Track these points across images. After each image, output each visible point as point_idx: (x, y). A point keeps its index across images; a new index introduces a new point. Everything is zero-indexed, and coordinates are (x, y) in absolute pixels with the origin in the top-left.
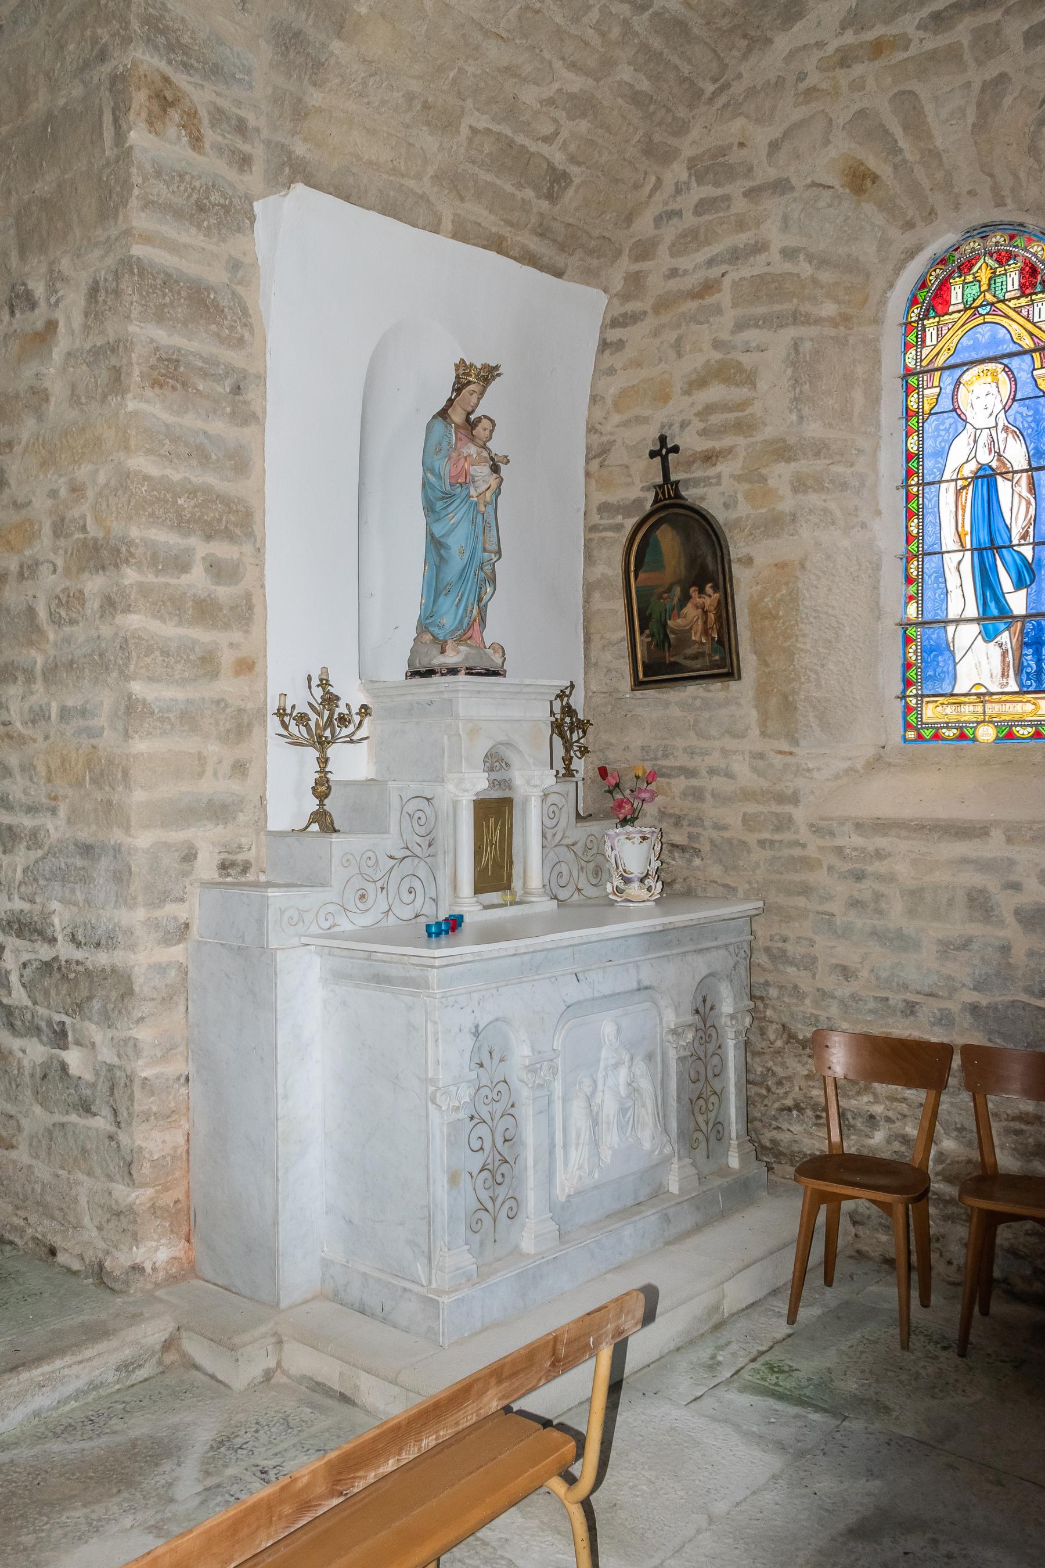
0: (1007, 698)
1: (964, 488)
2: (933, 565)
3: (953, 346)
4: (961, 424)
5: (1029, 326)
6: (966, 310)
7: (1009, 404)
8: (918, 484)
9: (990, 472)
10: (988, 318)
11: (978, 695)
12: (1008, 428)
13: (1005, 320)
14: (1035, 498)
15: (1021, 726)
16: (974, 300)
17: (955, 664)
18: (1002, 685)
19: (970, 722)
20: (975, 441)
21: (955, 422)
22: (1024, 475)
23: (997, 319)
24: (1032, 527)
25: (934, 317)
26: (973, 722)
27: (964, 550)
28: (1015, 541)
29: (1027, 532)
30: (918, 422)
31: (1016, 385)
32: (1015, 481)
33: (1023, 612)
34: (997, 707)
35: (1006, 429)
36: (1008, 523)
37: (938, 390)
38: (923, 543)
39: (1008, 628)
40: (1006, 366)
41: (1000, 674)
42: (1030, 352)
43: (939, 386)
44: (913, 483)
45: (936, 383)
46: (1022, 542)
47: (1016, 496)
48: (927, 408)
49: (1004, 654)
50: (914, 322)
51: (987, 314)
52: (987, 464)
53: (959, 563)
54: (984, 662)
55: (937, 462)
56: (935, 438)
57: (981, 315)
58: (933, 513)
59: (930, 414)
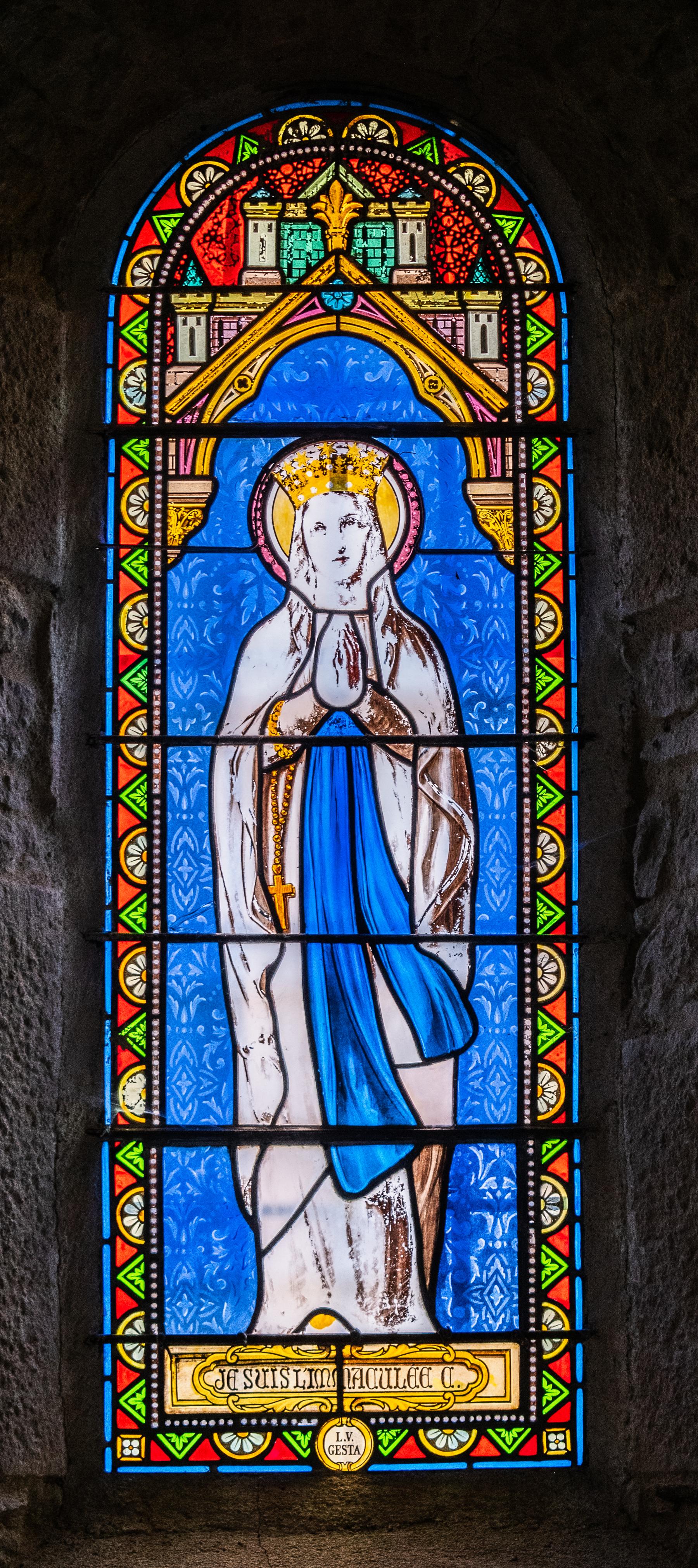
0: (402, 1350)
1: (280, 765)
2: (194, 971)
3: (256, 374)
4: (270, 591)
5: (458, 366)
6: (285, 289)
7: (402, 558)
8: (148, 740)
9: (352, 731)
10: (350, 324)
11: (323, 1341)
12: (400, 619)
13: (394, 337)
14: (475, 819)
15: (441, 1426)
16: (310, 270)
17: (260, 1254)
18: (388, 1317)
19: (300, 1416)
20: (314, 643)
21: (258, 581)
22: (446, 751)
23: (373, 331)
24: (467, 896)
25: (199, 291)
26: (309, 1416)
27: (280, 937)
28: (424, 929)
29: (455, 906)
30: (149, 564)
31: (421, 508)
32: (423, 762)
33: (446, 1121)
34: (375, 1375)
35: (394, 622)
36: (404, 874)
37: (205, 487)
38: (163, 907)
39: (406, 1163)
40: (394, 455)
41: (382, 1287)
42: (461, 431)
43: (211, 477)
44: (133, 732)
45: (202, 468)
46: (443, 931)
47: (425, 808)
48: (176, 531)
49: (394, 1234)
50: (143, 291)
51: (347, 311)
52: (347, 710)
53: (270, 971)
54: (340, 1252)
55: (205, 684)
56: (200, 617)
57: (329, 312)
58: (194, 825)
59: (185, 548)
